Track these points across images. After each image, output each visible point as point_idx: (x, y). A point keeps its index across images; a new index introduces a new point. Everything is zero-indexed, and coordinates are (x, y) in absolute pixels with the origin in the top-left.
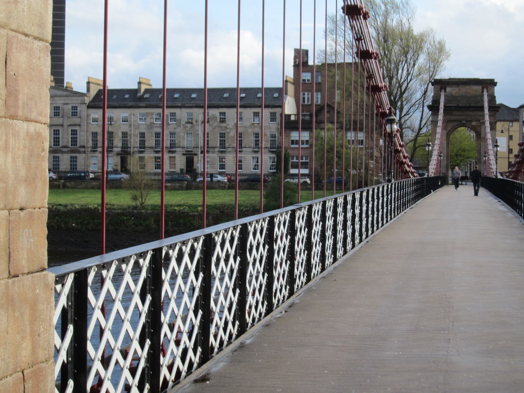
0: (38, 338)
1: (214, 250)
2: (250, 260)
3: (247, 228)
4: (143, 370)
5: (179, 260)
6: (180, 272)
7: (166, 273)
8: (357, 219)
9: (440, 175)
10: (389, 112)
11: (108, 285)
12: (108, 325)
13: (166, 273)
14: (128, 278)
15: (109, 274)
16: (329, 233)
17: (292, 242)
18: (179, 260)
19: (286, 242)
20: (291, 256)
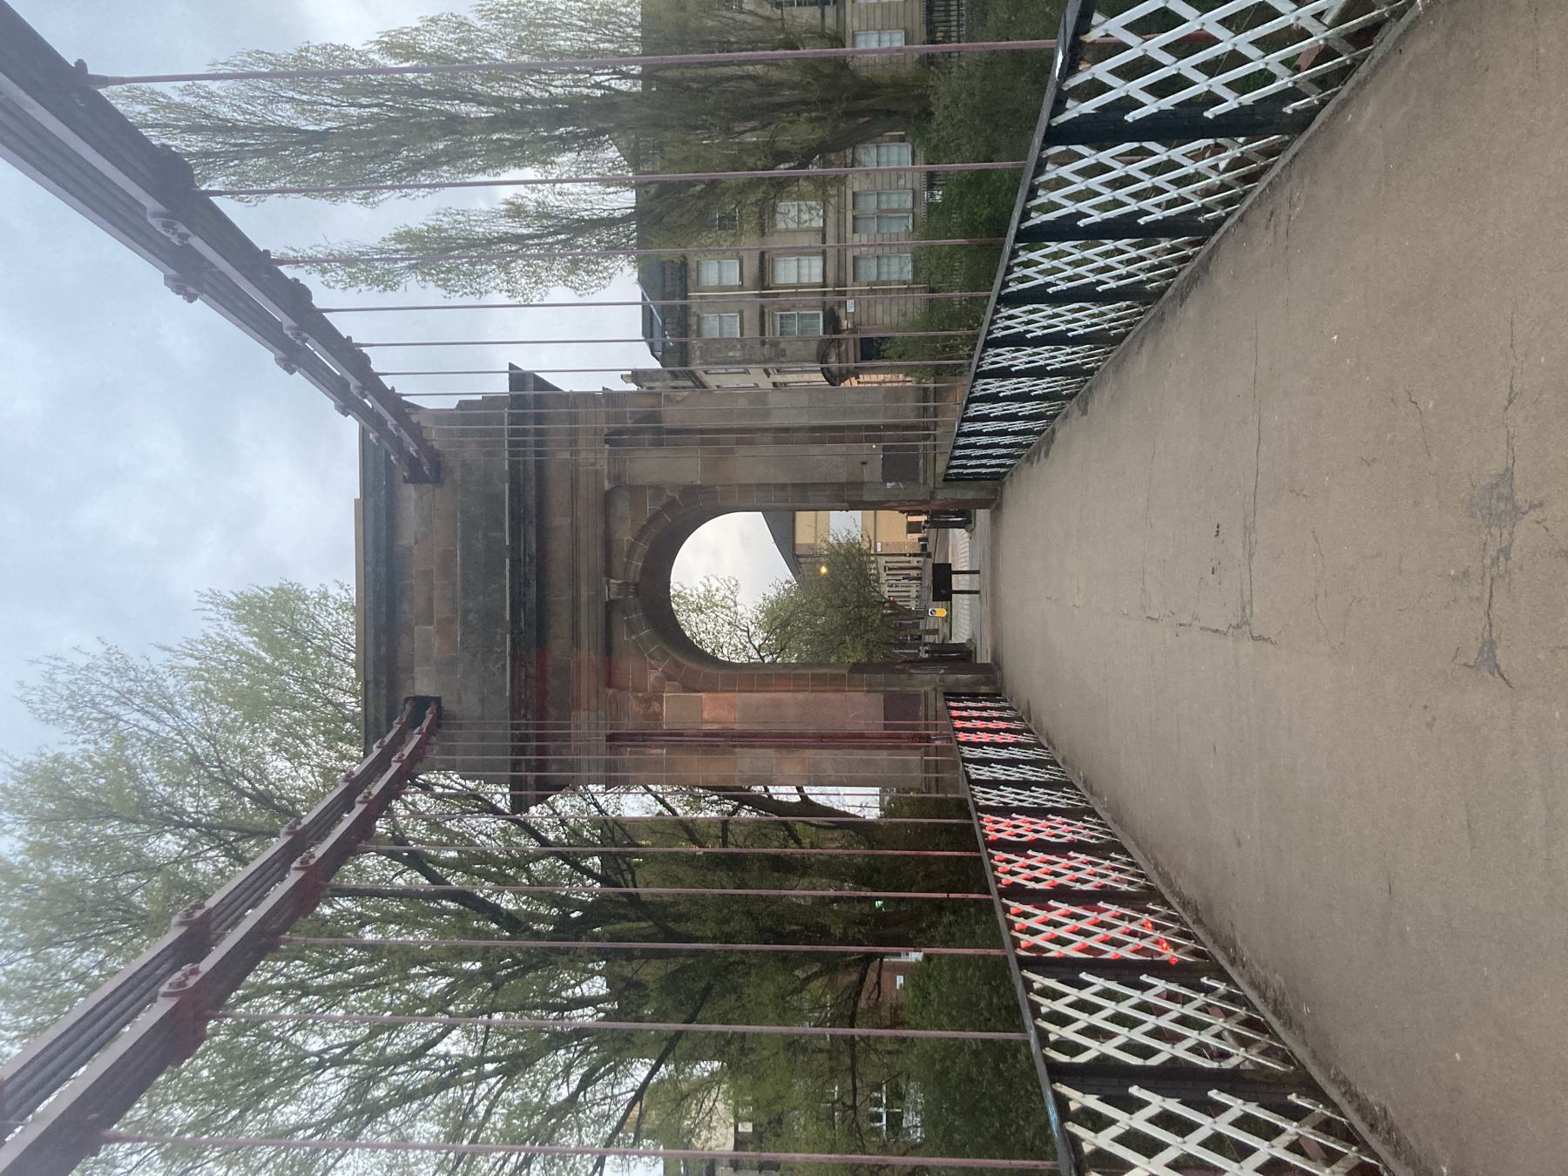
0: (941, 612)
1: (1020, 885)
2: (1031, 836)
3: (993, 841)
4: (1181, 985)
5: (1034, 932)
6: (1050, 931)
7: (1050, 951)
8: (985, 714)
9: (714, 1079)
10: (376, 1100)
11: (1069, 1033)
12: (1124, 1034)
13: (1050, 951)
14: (1059, 1006)
15: (1055, 1032)
16: (1004, 754)
17: (1007, 783)
18: (1034, 932)
19: (1021, 819)
20: (1025, 785)
